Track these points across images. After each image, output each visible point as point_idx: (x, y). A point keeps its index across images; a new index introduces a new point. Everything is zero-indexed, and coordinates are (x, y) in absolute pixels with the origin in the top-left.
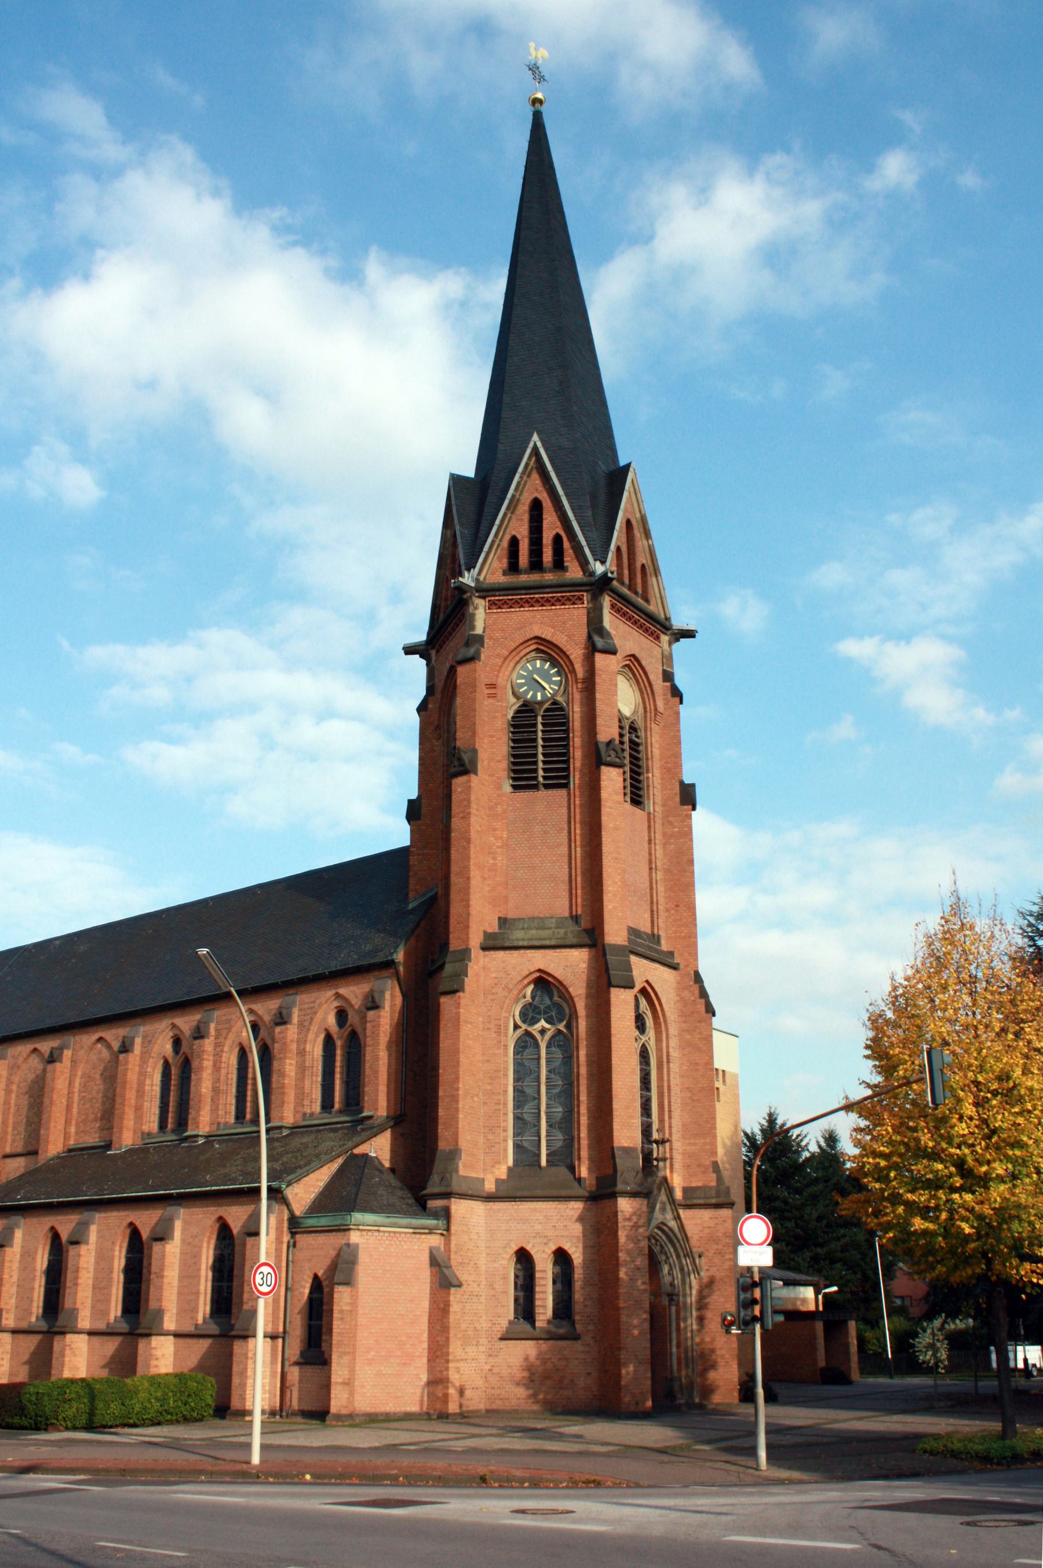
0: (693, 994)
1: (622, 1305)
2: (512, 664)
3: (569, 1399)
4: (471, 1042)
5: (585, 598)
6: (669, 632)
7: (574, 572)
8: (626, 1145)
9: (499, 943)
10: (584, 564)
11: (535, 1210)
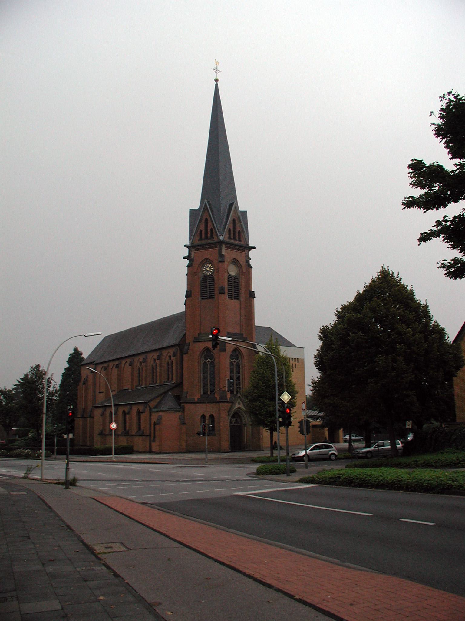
7: (216, 240)
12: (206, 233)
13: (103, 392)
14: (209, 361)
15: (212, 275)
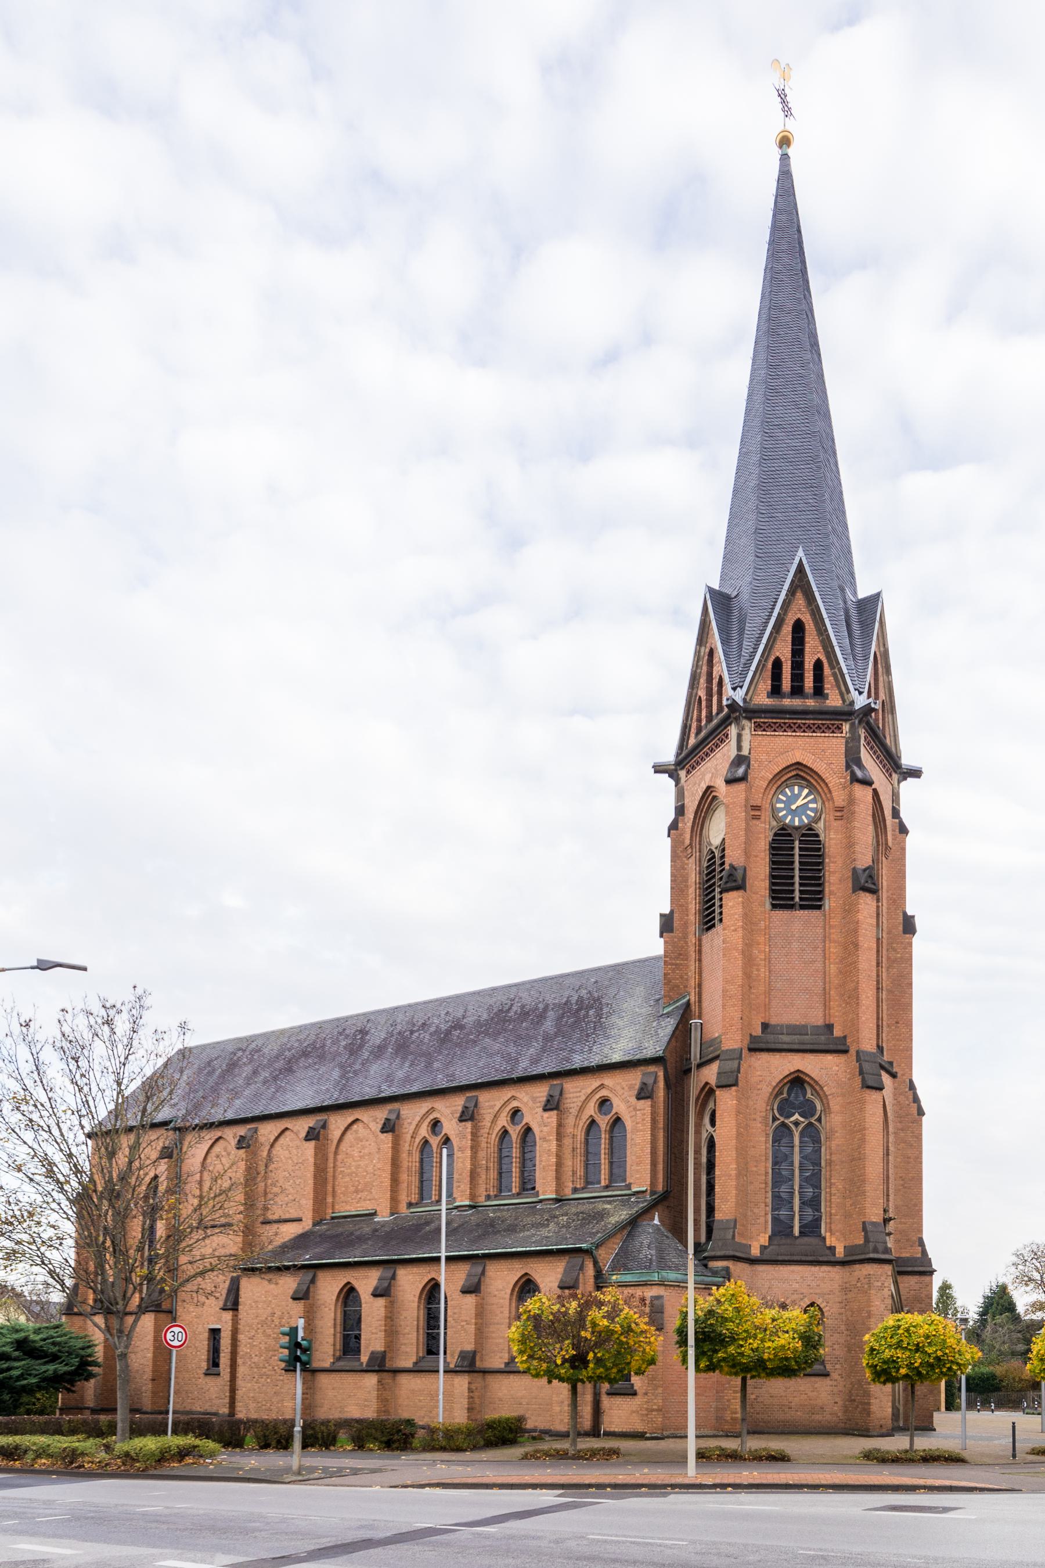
2: (774, 789)
6: (898, 771)
7: (834, 701)
10: (844, 692)
11: (793, 1272)
12: (798, 676)
13: (300, 1220)
14: (797, 1124)
15: (810, 829)
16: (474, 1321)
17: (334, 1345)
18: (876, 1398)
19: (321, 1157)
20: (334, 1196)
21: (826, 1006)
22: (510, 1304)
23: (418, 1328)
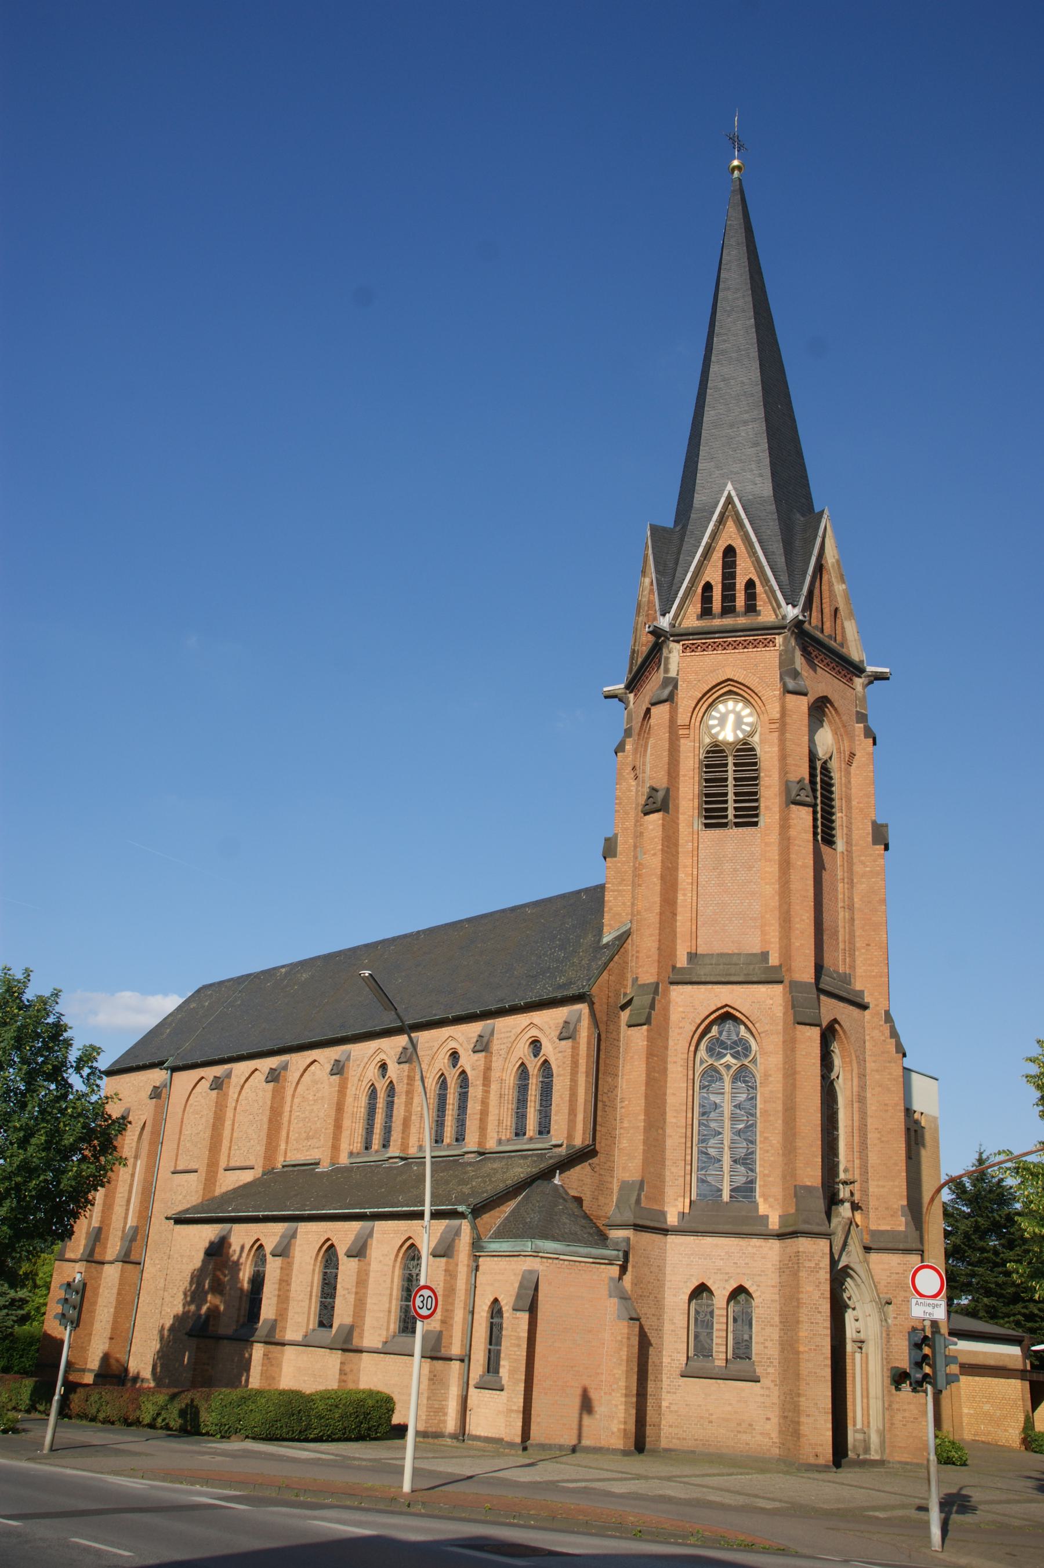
0: (883, 1034)
1: (801, 1349)
3: (747, 1444)
4: (657, 1075)
5: (777, 641)
8: (809, 1184)
9: (687, 978)
12: (728, 595)
16: (354, 1290)
17: (239, 1309)
18: (808, 1416)
19: (278, 1096)
20: (287, 1143)
21: (764, 933)
22: (393, 1272)
23: (311, 1295)
